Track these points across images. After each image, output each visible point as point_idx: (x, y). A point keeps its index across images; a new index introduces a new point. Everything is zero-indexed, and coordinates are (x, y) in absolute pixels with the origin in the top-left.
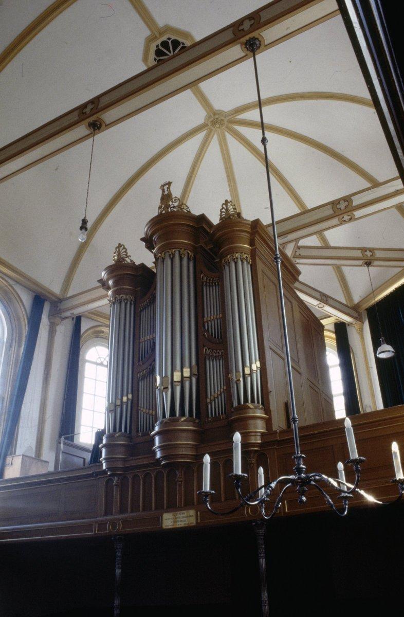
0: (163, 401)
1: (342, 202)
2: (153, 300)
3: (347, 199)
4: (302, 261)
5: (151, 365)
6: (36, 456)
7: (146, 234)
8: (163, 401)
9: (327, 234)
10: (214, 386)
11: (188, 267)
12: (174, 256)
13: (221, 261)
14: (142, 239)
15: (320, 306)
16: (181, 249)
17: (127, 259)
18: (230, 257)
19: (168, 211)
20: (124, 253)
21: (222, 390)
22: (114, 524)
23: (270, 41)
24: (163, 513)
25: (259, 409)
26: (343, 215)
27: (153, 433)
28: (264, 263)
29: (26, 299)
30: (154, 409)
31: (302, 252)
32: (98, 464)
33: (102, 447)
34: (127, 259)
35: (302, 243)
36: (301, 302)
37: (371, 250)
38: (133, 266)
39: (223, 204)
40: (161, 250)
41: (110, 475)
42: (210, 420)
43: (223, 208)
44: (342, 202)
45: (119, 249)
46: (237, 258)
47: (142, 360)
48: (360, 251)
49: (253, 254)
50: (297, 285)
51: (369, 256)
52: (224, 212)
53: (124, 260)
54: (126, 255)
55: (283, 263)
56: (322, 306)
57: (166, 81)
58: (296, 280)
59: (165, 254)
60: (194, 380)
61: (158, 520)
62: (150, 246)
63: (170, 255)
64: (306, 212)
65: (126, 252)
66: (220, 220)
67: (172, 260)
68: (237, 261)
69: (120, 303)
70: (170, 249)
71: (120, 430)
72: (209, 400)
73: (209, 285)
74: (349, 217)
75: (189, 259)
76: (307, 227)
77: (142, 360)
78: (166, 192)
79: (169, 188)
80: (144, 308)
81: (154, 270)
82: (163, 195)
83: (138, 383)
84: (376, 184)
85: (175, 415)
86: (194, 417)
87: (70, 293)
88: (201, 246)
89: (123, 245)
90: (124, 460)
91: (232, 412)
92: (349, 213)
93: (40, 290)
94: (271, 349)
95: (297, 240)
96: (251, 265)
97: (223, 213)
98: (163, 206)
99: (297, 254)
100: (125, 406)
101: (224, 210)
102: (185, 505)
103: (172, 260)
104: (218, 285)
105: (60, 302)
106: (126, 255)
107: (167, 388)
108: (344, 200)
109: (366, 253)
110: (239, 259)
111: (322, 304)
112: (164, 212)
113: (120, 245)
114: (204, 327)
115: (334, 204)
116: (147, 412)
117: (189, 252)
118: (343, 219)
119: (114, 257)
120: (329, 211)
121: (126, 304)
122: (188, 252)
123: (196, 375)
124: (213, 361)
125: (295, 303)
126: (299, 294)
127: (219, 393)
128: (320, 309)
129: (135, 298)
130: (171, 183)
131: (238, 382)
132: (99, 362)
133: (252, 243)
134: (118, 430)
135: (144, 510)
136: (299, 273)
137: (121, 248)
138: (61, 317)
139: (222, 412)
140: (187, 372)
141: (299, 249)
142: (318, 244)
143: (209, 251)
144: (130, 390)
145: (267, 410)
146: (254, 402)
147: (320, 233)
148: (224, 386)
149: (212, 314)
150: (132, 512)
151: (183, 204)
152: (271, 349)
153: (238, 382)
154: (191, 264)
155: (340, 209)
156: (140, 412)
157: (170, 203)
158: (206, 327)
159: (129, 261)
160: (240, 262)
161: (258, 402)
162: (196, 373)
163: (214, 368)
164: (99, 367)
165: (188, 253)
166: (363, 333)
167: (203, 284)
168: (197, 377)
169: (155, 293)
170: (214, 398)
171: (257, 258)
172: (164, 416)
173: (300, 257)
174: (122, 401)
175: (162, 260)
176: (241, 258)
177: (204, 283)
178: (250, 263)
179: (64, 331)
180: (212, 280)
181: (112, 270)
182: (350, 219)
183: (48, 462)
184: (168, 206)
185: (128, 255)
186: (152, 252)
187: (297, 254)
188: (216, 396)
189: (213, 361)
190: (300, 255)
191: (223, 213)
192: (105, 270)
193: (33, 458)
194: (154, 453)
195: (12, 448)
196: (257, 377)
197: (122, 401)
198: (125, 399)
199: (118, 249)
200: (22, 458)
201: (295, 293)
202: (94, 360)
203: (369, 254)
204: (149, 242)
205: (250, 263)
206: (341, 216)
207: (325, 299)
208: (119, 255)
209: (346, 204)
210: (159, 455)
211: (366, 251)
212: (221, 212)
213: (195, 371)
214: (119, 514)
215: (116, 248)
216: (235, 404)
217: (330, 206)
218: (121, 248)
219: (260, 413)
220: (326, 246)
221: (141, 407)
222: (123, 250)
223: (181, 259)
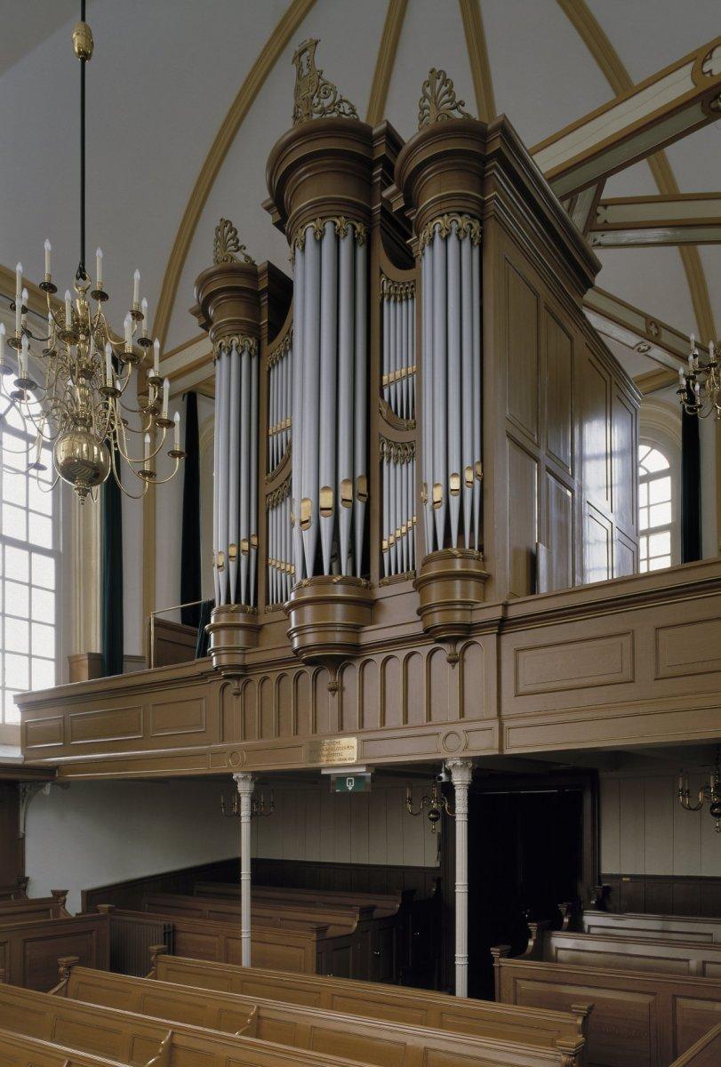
4: (609, 237)
15: (642, 348)
21: (410, 524)
31: (606, 215)
33: (210, 630)
36: (593, 333)
38: (250, 271)
43: (426, 96)
50: (590, 296)
52: (427, 108)
56: (646, 348)
57: (571, 160)
58: (590, 285)
60: (360, 506)
67: (319, 242)
71: (238, 600)
77: (273, 469)
83: (267, 513)
95: (600, 182)
99: (600, 220)
100: (244, 558)
103: (319, 242)
114: (383, 397)
117: (355, 223)
123: (365, 496)
125: (580, 340)
126: (593, 319)
134: (232, 602)
136: (595, 267)
139: (335, 556)
148: (413, 516)
154: (361, 252)
155: (710, 71)
156: (270, 568)
162: (365, 492)
165: (354, 228)
168: (365, 499)
170: (396, 539)
173: (608, 227)
185: (240, 244)
190: (606, 222)
201: (583, 316)
213: (362, 488)
215: (218, 229)
220: (671, 195)
223: (337, 239)
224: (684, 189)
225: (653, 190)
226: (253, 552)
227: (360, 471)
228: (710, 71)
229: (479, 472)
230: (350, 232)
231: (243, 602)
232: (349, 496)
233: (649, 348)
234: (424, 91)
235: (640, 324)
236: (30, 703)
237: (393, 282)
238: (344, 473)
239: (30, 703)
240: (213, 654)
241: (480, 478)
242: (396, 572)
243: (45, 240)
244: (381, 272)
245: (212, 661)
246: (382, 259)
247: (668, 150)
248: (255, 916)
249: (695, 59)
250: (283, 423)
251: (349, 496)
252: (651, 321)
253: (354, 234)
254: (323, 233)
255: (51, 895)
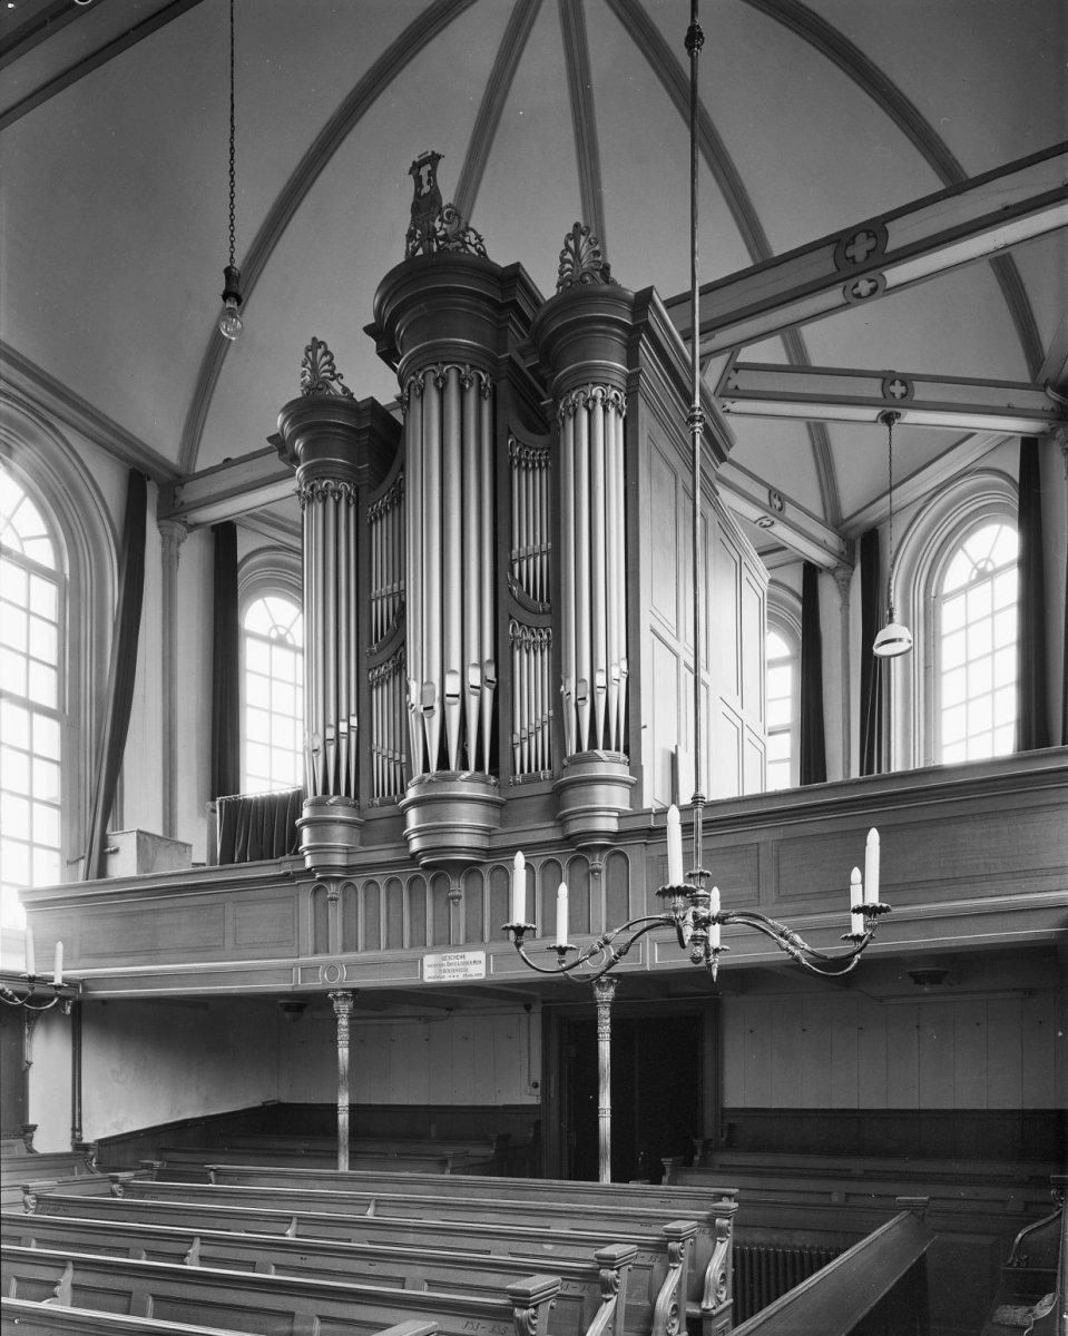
0: (425, 735)
1: (861, 238)
2: (398, 498)
3: (875, 228)
5: (395, 654)
6: (164, 834)
7: (378, 313)
8: (425, 735)
9: (808, 332)
10: (530, 710)
11: (479, 415)
12: (446, 383)
13: (555, 404)
14: (369, 330)
15: (765, 522)
16: (464, 364)
17: (334, 384)
18: (577, 396)
19: (431, 248)
20: (326, 367)
21: (546, 719)
22: (332, 969)
23: (894, 284)
24: (424, 954)
25: (618, 762)
26: (854, 281)
27: (404, 802)
28: (654, 412)
29: (109, 481)
30: (404, 751)
31: (744, 381)
32: (299, 857)
33: (302, 825)
34: (334, 384)
35: (747, 355)
37: (906, 380)
38: (348, 405)
39: (569, 235)
40: (415, 365)
41: (320, 879)
42: (519, 778)
43: (568, 248)
44: (861, 238)
45: (315, 355)
46: (594, 399)
47: (376, 641)
48: (877, 383)
49: (632, 388)
51: (898, 395)
52: (569, 262)
53: (328, 387)
54: (332, 372)
55: (707, 431)
56: (769, 523)
58: (722, 458)
59: (424, 377)
60: (488, 694)
61: (417, 963)
62: (388, 355)
63: (436, 380)
64: (766, 264)
65: (330, 363)
66: (558, 285)
67: (442, 392)
68: (594, 406)
69: (325, 499)
70: (436, 364)
71: (337, 792)
72: (517, 739)
73: (527, 465)
74: (872, 285)
75: (480, 395)
76: (771, 308)
77: (376, 641)
78: (426, 189)
79: (432, 174)
80: (378, 517)
81: (398, 415)
82: (417, 195)
84: (957, 184)
85: (448, 768)
86: (487, 773)
87: (200, 466)
88: (510, 358)
89: (323, 343)
90: (349, 852)
91: (564, 767)
92: (871, 275)
93: (142, 459)
94: (653, 631)
95: (734, 348)
96: (625, 420)
97: (568, 266)
98: (419, 232)
99: (731, 385)
100: (343, 742)
101: (569, 256)
102: (467, 940)
103: (442, 392)
104: (547, 465)
105: (182, 485)
106: (332, 372)
107: (431, 708)
108: (867, 232)
109: (892, 388)
110: (599, 401)
111: (770, 517)
112: (420, 252)
113: (316, 344)
115: (840, 241)
116: (397, 758)
118: (855, 291)
119: (304, 374)
120: (823, 264)
121: (337, 503)
122: (479, 375)
124: (528, 652)
127: (539, 725)
128: (764, 530)
129: (357, 492)
130: (439, 157)
131: (580, 703)
132: (274, 635)
133: (632, 359)
134: (331, 793)
135: (388, 947)
137: (320, 352)
138: (185, 522)
140: (474, 677)
141: (736, 370)
142: (782, 359)
143: (526, 372)
144: (353, 710)
145: (636, 768)
146: (609, 749)
147: (790, 331)
149: (529, 535)
150: (366, 948)
151: (468, 229)
152: (653, 631)
153: (580, 703)
155: (853, 257)
157: (437, 224)
158: (517, 576)
159: (339, 389)
160: (600, 409)
161: (618, 749)
163: (530, 670)
164: (277, 651)
165: (480, 379)
166: (848, 592)
167: (512, 462)
169: (404, 480)
171: (641, 401)
172: (426, 768)
173: (738, 394)
174: (337, 732)
175: (418, 392)
176: (602, 399)
177: (524, 464)
178: (624, 413)
179: (194, 555)
180: (534, 455)
181: (295, 410)
182: (873, 291)
183: (191, 846)
184: (431, 235)
185: (336, 372)
186: (394, 369)
187: (731, 385)
188: (532, 729)
189: (528, 652)
190: (737, 387)
191: (568, 266)
192: (286, 409)
193: (159, 837)
194: (406, 841)
195: (115, 814)
196: (618, 693)
197: (337, 732)
198: (343, 727)
199: (310, 354)
200: (138, 837)
202: (264, 633)
203: (898, 389)
204: (385, 337)
205: (624, 413)
206: (852, 282)
207: (778, 504)
208: (314, 370)
209: (871, 244)
210: (415, 845)
211: (893, 383)
212: (564, 262)
213: (490, 674)
214: (341, 953)
215: (308, 349)
216: (572, 749)
217: (828, 251)
218: (320, 352)
219: (621, 771)
220: (800, 365)
221: (377, 744)
222: (325, 359)
223: (462, 391)
224: (816, 362)
225: (783, 360)
226: (353, 735)
227: (488, 655)
228: (853, 257)
229: (625, 669)
230: (475, 382)
231: (343, 794)
232: (477, 683)
233: (773, 523)
234: (566, 244)
235: (763, 495)
236: (41, 903)
237: (525, 446)
238: (474, 658)
239: (41, 903)
240: (306, 853)
241: (625, 675)
242: (529, 770)
243: (869, 829)
244: (510, 432)
245: (304, 859)
246: (511, 419)
247: (747, 263)
248: (739, 1226)
249: (839, 241)
250: (390, 587)
251: (477, 683)
252: (773, 492)
253: (480, 386)
254: (445, 379)
255: (31, 1121)
